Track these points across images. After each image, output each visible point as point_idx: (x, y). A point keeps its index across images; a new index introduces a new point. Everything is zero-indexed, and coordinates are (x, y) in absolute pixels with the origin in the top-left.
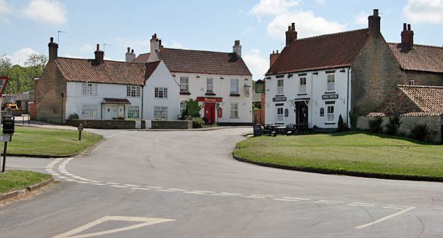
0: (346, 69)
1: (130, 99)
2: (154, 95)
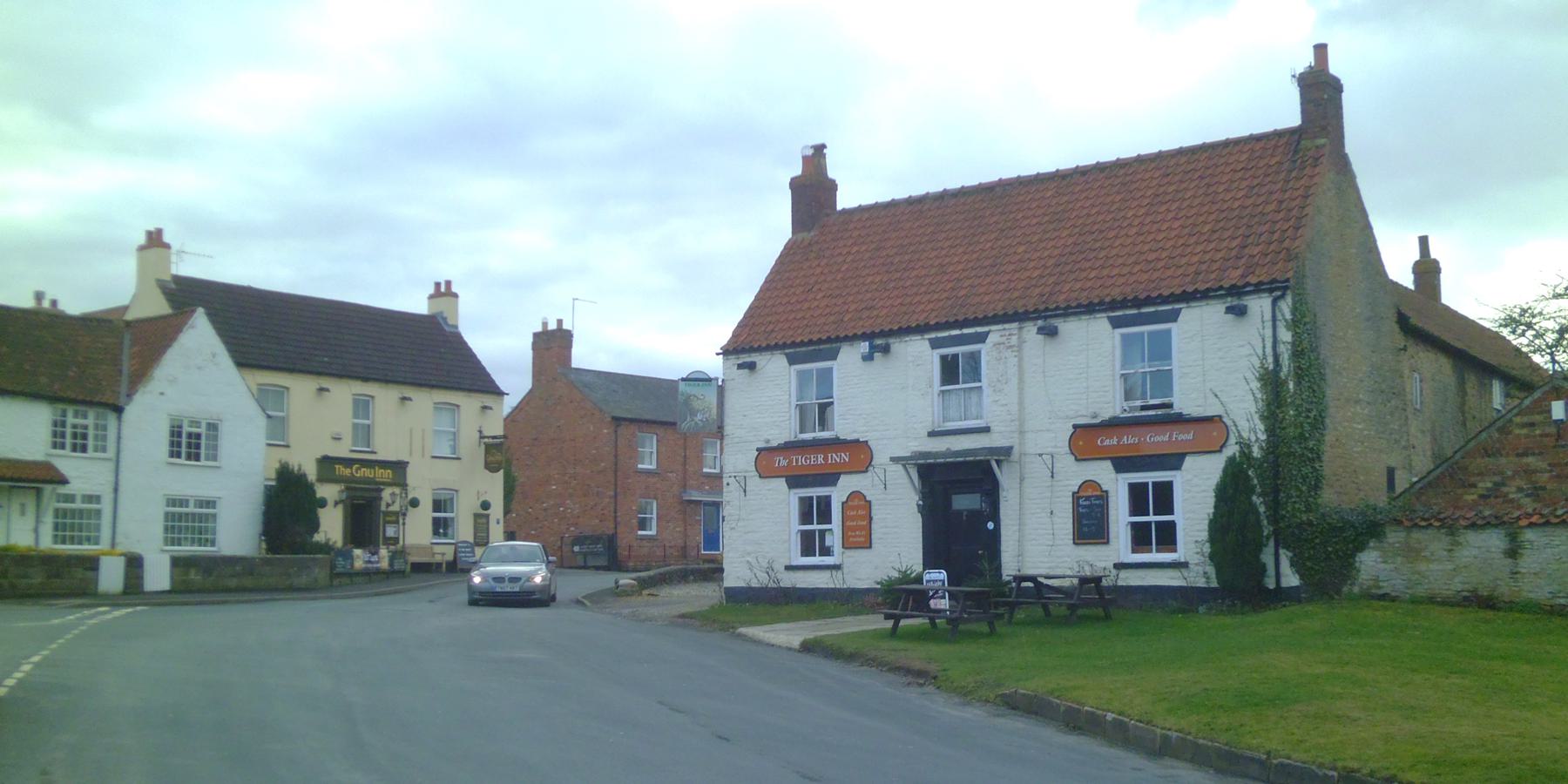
0: (1260, 305)
1: (67, 463)
2: (164, 448)
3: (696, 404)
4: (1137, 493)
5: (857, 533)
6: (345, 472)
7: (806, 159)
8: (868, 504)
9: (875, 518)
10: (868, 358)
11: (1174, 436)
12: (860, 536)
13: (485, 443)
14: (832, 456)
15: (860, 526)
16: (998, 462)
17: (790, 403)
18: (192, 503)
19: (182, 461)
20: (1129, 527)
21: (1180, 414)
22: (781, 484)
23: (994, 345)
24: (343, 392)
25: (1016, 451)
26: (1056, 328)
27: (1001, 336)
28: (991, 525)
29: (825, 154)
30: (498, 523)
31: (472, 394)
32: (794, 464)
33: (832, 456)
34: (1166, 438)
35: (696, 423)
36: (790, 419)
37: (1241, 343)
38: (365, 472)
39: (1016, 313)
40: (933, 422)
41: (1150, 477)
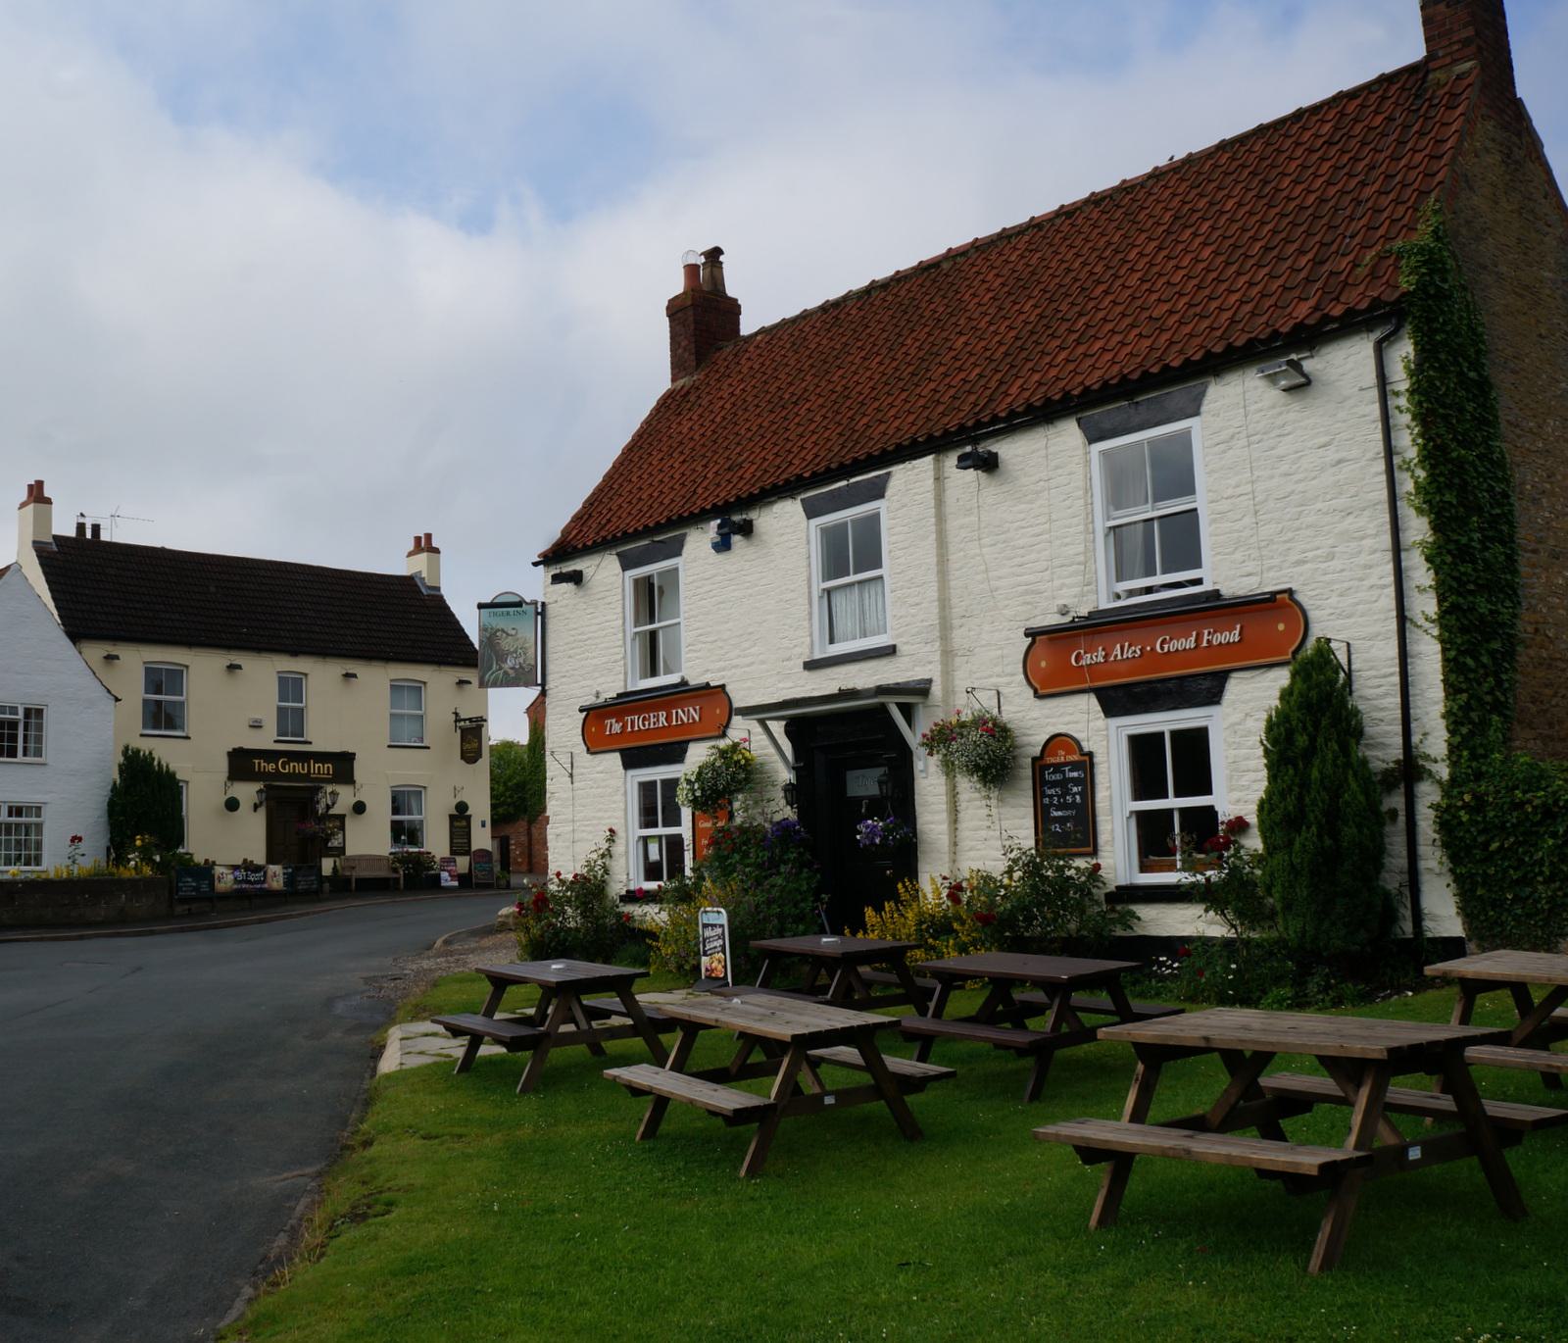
3: (506, 644)
4: (1144, 751)
7: (691, 270)
10: (723, 545)
11: (1206, 637)
17: (624, 631)
20: (1133, 822)
21: (1216, 594)
22: (615, 759)
24: (263, 672)
25: (936, 689)
26: (995, 456)
29: (721, 263)
30: (483, 825)
31: (443, 668)
32: (629, 729)
34: (1190, 643)
35: (506, 673)
36: (624, 658)
37: (1323, 440)
39: (930, 437)
41: (1164, 722)
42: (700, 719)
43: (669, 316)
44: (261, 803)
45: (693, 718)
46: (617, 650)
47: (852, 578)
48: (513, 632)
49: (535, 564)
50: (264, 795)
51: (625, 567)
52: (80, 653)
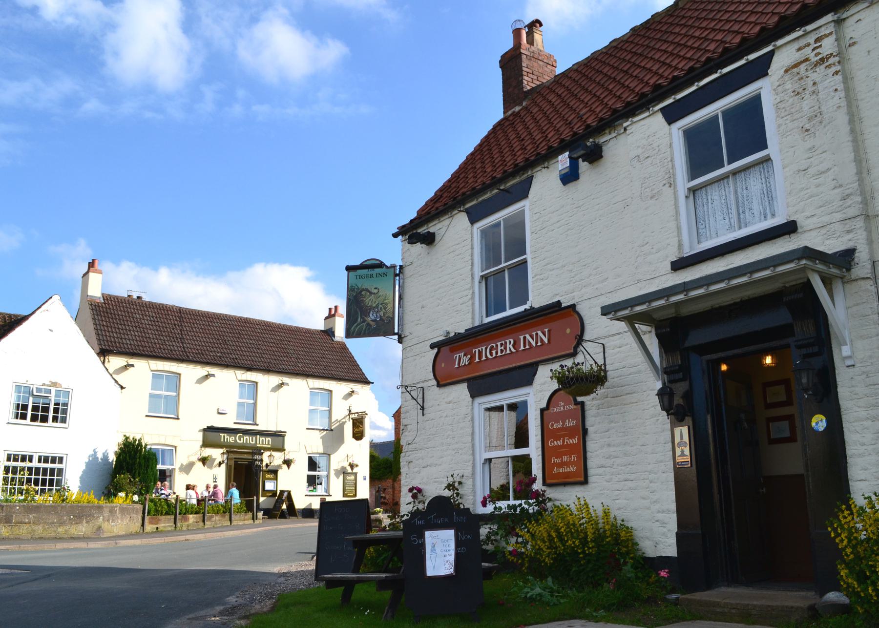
3: (369, 301)
5: (565, 459)
6: (230, 439)
8: (579, 407)
9: (591, 430)
10: (570, 177)
12: (567, 464)
13: (352, 418)
14: (525, 338)
15: (568, 445)
16: (827, 281)
18: (35, 459)
19: (38, 423)
22: (461, 391)
23: (786, 71)
27: (799, 49)
28: (819, 422)
30: (365, 479)
32: (477, 360)
33: (525, 338)
35: (368, 324)
38: (249, 440)
40: (680, 245)
42: (549, 340)
43: (500, 67)
44: (223, 462)
45: (542, 340)
46: (465, 293)
47: (728, 168)
48: (376, 291)
49: (395, 236)
50: (225, 456)
51: (473, 221)
52: (103, 363)
